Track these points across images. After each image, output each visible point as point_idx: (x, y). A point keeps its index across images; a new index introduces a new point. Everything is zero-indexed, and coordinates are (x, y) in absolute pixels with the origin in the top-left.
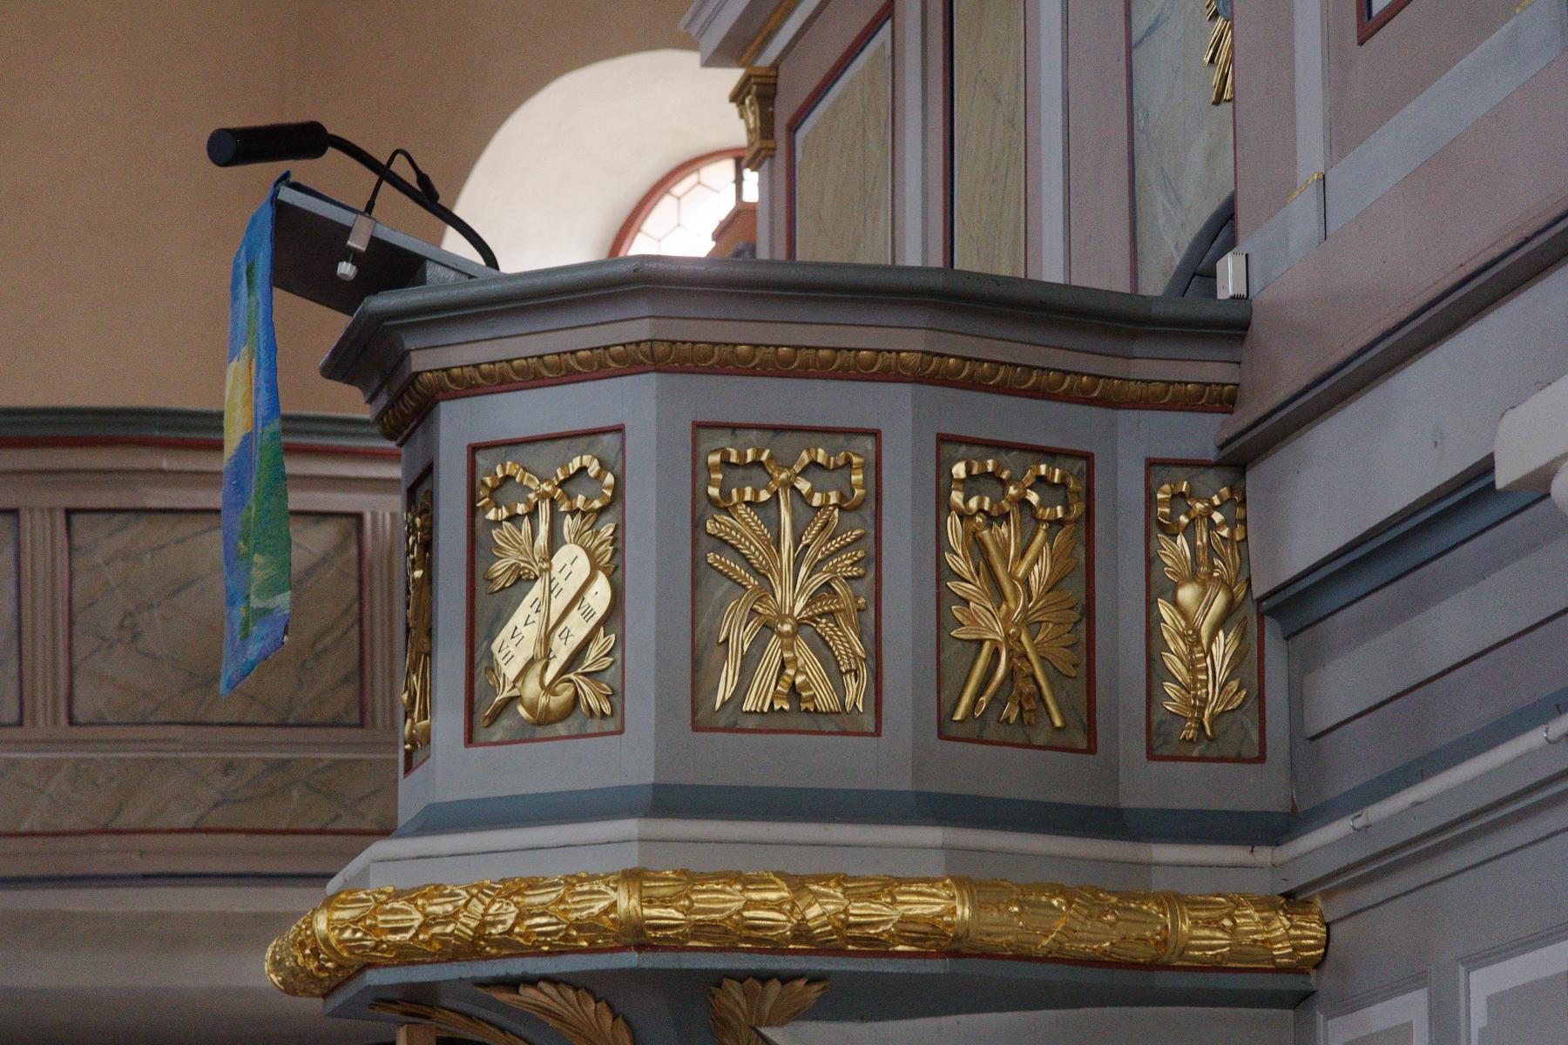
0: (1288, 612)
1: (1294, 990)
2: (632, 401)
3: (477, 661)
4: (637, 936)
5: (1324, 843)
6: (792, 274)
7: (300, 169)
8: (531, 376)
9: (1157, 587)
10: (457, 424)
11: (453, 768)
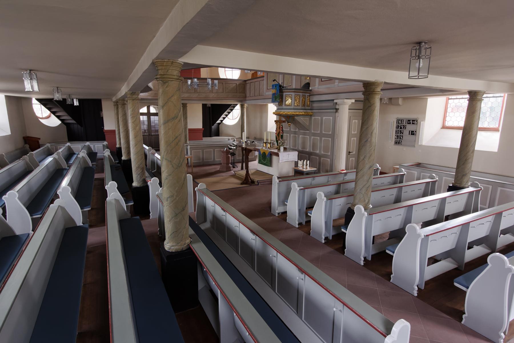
1: (311, 116)
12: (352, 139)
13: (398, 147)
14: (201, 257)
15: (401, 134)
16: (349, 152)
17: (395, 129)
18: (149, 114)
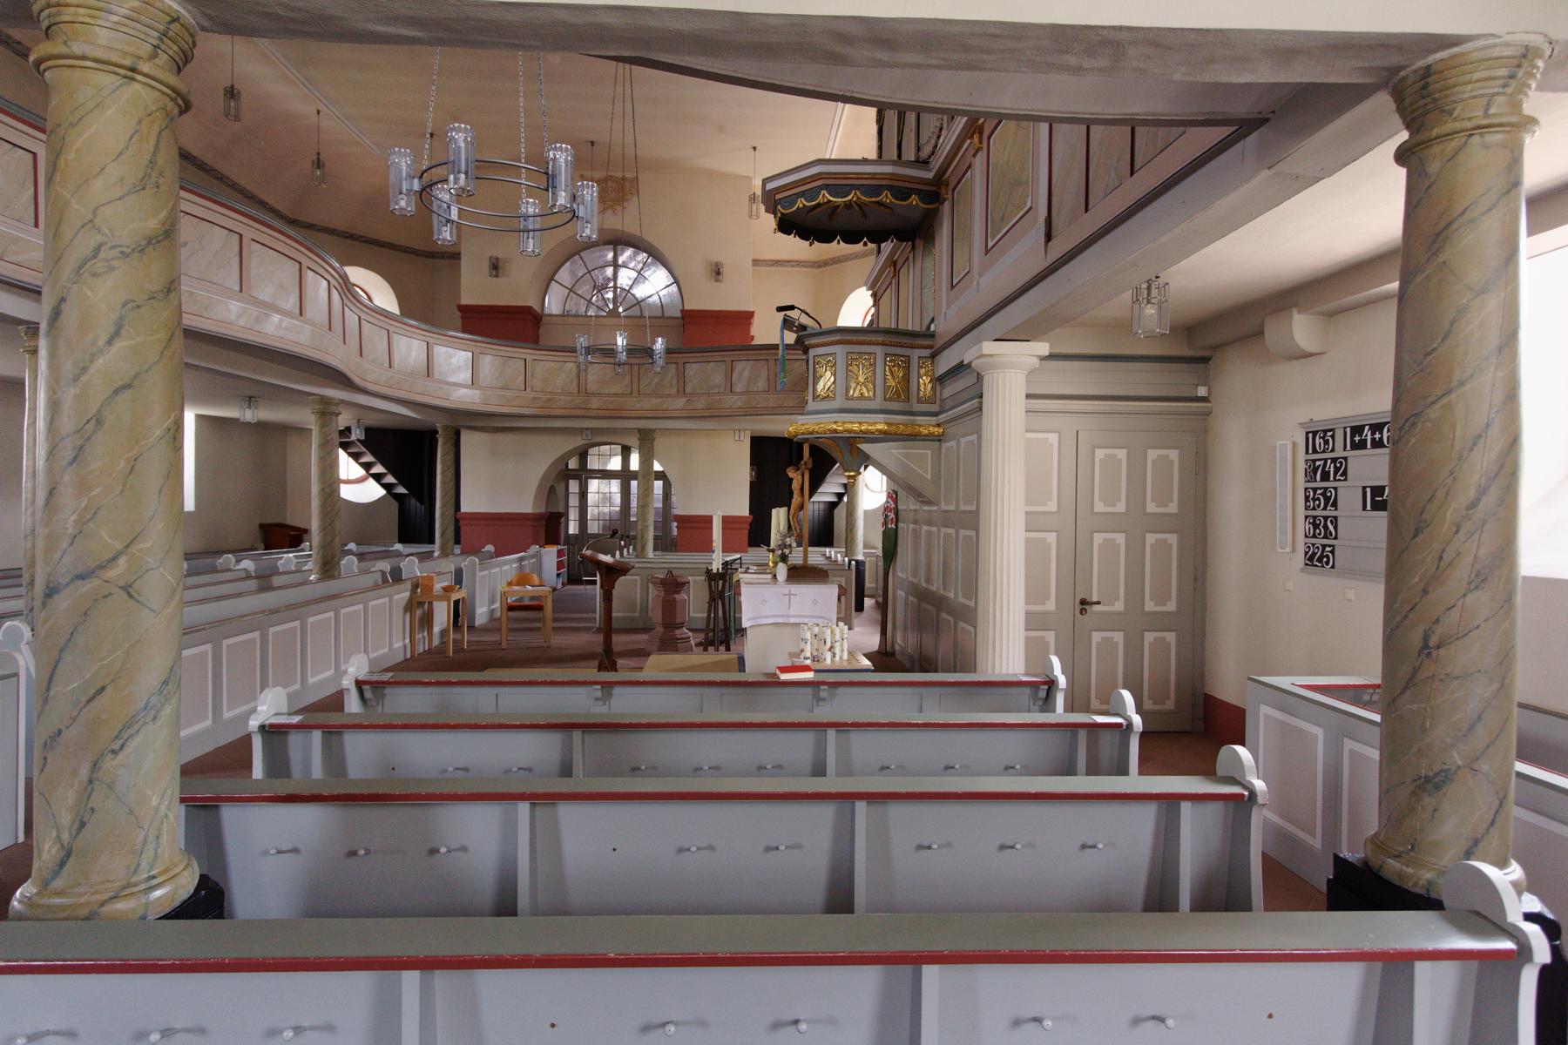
0: (940, 380)
1: (939, 439)
4: (835, 431)
5: (942, 417)
7: (789, 313)
8: (823, 345)
9: (920, 376)
10: (812, 352)
11: (811, 406)
12: (1098, 538)
13: (1321, 580)
14: (159, 955)
15: (1330, 512)
16: (1083, 602)
17: (1301, 483)
18: (625, 476)
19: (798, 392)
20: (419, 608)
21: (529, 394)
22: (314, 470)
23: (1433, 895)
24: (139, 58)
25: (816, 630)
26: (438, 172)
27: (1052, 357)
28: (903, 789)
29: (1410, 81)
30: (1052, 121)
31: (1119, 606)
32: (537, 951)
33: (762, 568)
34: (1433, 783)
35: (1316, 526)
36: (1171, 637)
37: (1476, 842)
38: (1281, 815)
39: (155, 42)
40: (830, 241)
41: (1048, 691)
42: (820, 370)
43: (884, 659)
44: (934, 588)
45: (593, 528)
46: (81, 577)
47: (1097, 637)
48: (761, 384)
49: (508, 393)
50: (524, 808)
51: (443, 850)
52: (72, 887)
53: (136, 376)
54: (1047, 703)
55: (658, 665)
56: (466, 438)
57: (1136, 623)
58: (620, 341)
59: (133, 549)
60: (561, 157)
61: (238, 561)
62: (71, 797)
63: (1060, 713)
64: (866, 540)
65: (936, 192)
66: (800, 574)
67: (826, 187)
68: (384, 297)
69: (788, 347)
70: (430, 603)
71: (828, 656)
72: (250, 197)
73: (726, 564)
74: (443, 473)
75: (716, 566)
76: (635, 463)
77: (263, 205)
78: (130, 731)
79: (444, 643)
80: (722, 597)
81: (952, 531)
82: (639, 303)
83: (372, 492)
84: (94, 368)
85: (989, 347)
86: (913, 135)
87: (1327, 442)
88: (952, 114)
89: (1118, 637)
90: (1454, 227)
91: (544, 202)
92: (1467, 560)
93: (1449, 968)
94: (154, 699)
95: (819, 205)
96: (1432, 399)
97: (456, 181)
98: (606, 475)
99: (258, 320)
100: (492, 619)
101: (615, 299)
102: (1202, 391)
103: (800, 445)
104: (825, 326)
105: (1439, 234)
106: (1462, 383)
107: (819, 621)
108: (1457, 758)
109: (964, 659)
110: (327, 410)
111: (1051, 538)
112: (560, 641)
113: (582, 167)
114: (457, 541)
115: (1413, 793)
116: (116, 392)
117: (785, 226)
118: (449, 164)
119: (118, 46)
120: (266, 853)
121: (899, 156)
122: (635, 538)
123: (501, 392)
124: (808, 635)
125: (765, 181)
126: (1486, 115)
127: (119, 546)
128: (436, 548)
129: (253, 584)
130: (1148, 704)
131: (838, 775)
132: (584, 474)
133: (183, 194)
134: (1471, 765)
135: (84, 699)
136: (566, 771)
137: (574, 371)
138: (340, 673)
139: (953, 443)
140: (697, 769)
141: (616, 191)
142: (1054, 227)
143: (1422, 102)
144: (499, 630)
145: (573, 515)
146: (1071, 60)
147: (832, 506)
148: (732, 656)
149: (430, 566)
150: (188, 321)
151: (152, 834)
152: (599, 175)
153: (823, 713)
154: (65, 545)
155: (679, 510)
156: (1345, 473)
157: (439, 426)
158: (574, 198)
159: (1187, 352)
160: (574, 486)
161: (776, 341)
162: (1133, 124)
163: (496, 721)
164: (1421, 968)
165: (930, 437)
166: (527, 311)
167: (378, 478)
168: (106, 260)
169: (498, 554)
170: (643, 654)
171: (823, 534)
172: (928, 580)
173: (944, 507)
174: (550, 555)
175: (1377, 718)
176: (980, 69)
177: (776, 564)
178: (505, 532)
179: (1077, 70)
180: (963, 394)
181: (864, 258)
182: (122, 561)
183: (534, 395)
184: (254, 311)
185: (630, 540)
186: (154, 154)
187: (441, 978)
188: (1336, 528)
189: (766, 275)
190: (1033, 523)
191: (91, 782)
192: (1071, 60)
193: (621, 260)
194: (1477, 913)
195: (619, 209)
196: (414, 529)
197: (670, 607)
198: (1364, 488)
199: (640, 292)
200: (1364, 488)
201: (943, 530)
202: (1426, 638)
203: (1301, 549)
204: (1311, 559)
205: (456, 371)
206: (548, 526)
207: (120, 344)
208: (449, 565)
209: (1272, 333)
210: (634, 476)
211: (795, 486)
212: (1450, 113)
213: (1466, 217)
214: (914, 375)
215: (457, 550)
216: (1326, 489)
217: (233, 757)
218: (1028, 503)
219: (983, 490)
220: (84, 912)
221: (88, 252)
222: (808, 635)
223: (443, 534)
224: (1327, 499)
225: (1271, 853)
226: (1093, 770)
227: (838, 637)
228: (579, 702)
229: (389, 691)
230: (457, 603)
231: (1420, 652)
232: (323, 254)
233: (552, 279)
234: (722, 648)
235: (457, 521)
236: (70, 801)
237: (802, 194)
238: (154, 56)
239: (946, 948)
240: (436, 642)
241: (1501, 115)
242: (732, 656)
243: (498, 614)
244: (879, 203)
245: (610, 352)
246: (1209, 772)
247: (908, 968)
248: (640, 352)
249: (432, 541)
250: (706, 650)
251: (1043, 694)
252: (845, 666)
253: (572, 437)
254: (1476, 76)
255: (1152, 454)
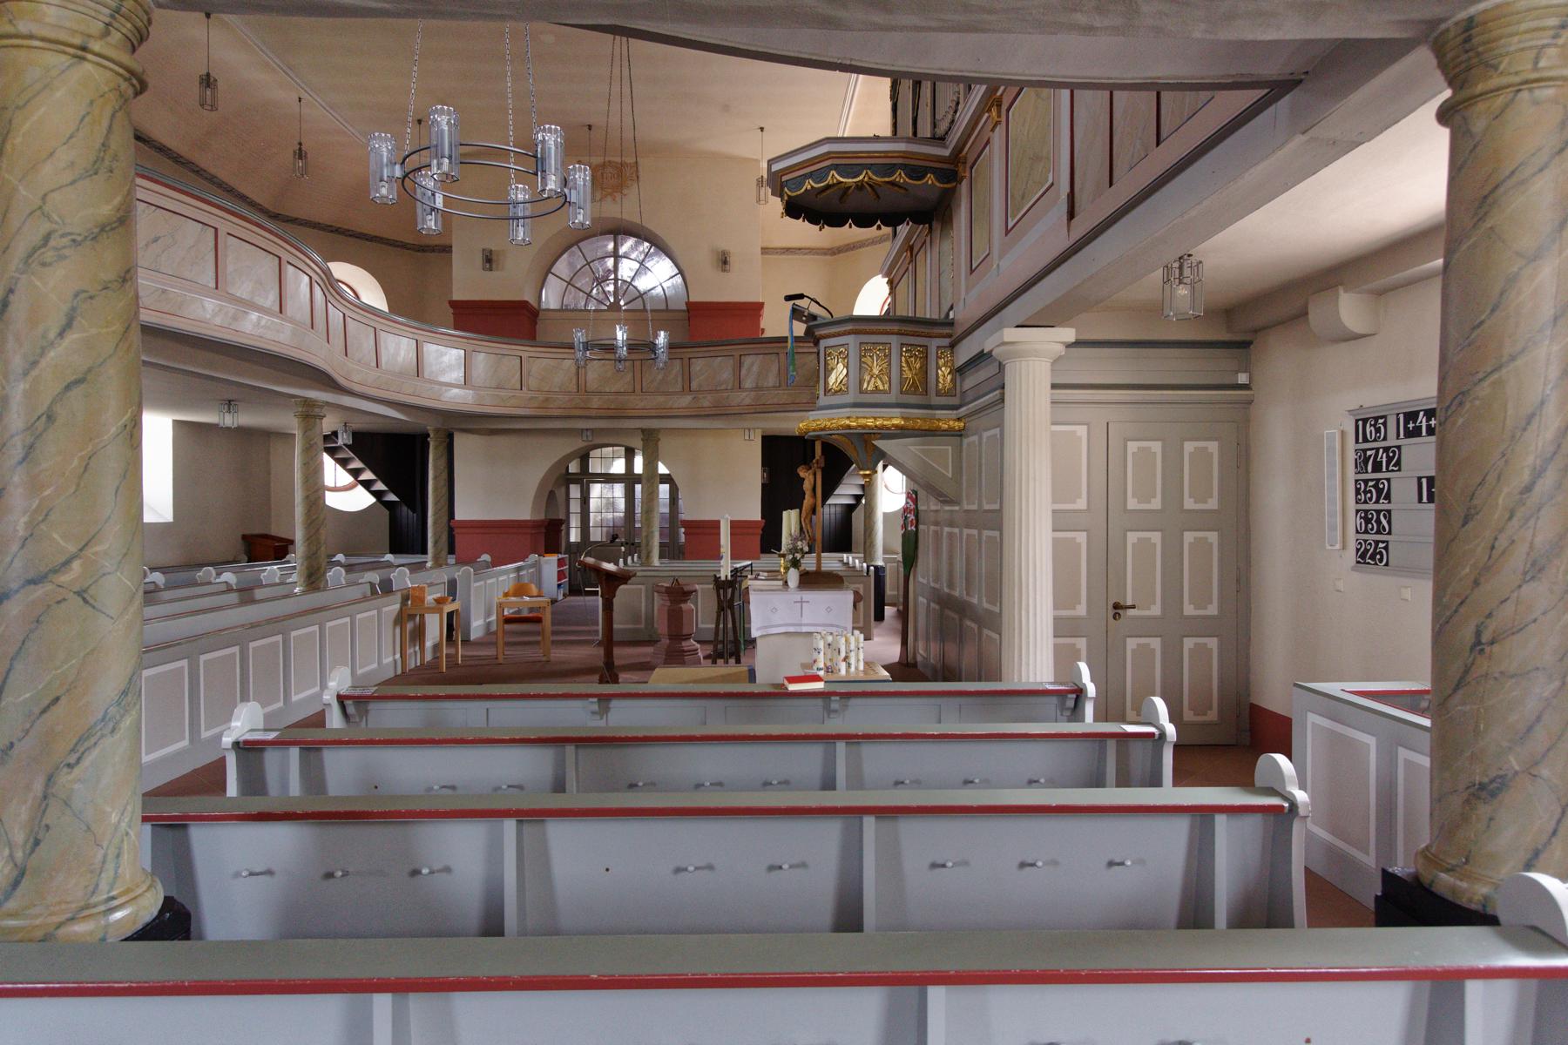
0: (960, 371)
1: (960, 434)
2: (850, 339)
3: (826, 383)
4: (849, 427)
6: (736, 351)
7: (798, 302)
8: (834, 335)
9: (938, 368)
10: (823, 343)
12: (1132, 537)
13: (1375, 579)
16: (1116, 606)
18: (629, 479)
19: (809, 387)
20: (410, 621)
21: (525, 394)
22: (298, 476)
23: (1490, 911)
24: (90, 36)
25: (830, 639)
26: (423, 157)
27: (1078, 344)
28: (914, 803)
29: (1452, 34)
30: (1073, 88)
31: (1156, 610)
32: (515, 972)
33: (773, 574)
34: (1486, 791)
35: (1368, 521)
36: (1213, 643)
37: (1537, 854)
38: (1333, 831)
39: (107, 20)
40: (841, 224)
41: (1077, 700)
42: (832, 363)
43: (904, 669)
44: (957, 593)
45: (596, 535)
46: (33, 582)
47: (1132, 643)
48: (771, 380)
49: (503, 393)
50: (510, 825)
51: (425, 871)
52: (27, 908)
53: (90, 370)
54: (1076, 713)
55: (665, 677)
56: (462, 443)
57: (1173, 627)
58: (621, 335)
59: (89, 552)
60: (551, 139)
61: (219, 574)
62: (24, 815)
63: (1090, 720)
64: (884, 545)
65: (952, 171)
66: (813, 580)
67: (836, 167)
68: (373, 295)
69: (797, 339)
70: (422, 616)
71: (843, 666)
72: (230, 191)
73: (735, 571)
74: (435, 478)
75: (725, 572)
76: (639, 466)
77: (243, 198)
78: (86, 744)
79: (436, 658)
80: (731, 607)
81: (975, 532)
82: (641, 295)
83: (361, 500)
84: (43, 363)
85: (1010, 334)
86: (928, 110)
87: (1378, 430)
88: (969, 83)
89: (1155, 643)
90: (1502, 189)
91: (533, 186)
92: (1521, 551)
93: (1505, 987)
94: (113, 710)
95: (828, 187)
96: (1480, 375)
97: (439, 165)
98: (610, 479)
99: (235, 318)
100: (488, 632)
101: (616, 293)
102: (1242, 378)
103: (812, 442)
104: (838, 315)
105: (1485, 197)
106: (1513, 358)
107: (834, 630)
108: (1514, 763)
109: (989, 668)
110: (310, 413)
111: (1081, 538)
112: (559, 654)
113: (573, 150)
114: (451, 551)
115: (1467, 801)
116: (68, 388)
117: (794, 209)
118: (428, 148)
119: (68, 24)
120: (237, 875)
121: (915, 133)
122: (639, 545)
123: (496, 392)
124: (821, 645)
125: (770, 163)
126: (1535, 68)
127: (72, 548)
128: (429, 559)
129: (233, 597)
130: (1188, 716)
131: (849, 788)
132: (585, 478)
133: (139, 181)
134: (1531, 770)
135: (37, 711)
136: (559, 786)
137: (573, 369)
138: (323, 686)
139: (975, 438)
140: (698, 786)
141: (614, 175)
142: (1077, 205)
143: (1464, 57)
144: (495, 644)
145: (575, 522)
146: (1081, 18)
147: (850, 509)
148: (743, 668)
149: (422, 577)
150: (146, 317)
151: (112, 852)
152: (597, 160)
153: (833, 726)
154: (15, 548)
155: (685, 515)
156: (1398, 463)
157: (430, 429)
158: (565, 182)
159: (1226, 337)
160: (575, 491)
161: (786, 334)
162: (1157, 89)
163: (485, 736)
164: (1473, 988)
165: (951, 433)
166: (523, 306)
167: (367, 485)
168: (57, 249)
169: (495, 564)
170: (648, 667)
171: (841, 537)
172: (951, 585)
173: (966, 507)
174: (550, 565)
175: (1427, 722)
176: (983, 31)
177: (787, 569)
178: (504, 540)
179: (1089, 30)
180: (981, 389)
181: (879, 241)
182: (76, 565)
183: (531, 394)
184: (231, 308)
185: (633, 547)
186: (107, 137)
187: (415, 1001)
188: (1389, 523)
189: (773, 262)
190: (1061, 521)
191: (45, 797)
192: (1081, 18)
193: (622, 250)
194: (1534, 928)
195: (618, 195)
196: (404, 536)
197: (676, 618)
198: (1420, 479)
199: (642, 284)
200: (1420, 479)
201: (966, 531)
202: (1478, 634)
203: (1352, 546)
204: (1363, 556)
205: (448, 369)
206: (549, 534)
207: (73, 337)
208: (443, 575)
209: (1317, 315)
210: (638, 479)
211: (807, 486)
212: (1495, 67)
213: (1514, 179)
214: (932, 365)
215: (451, 560)
216: (1378, 480)
217: (209, 779)
218: (1054, 502)
219: (1006, 484)
220: (39, 934)
221: (37, 239)
222: (821, 645)
223: (436, 543)
224: (1379, 492)
225: (1318, 869)
226: (1124, 781)
227: (853, 647)
228: (574, 715)
229: (372, 706)
230: (450, 615)
231: (1472, 649)
232: (304, 248)
233: (549, 271)
234: (732, 661)
235: (451, 532)
236: (24, 816)
237: (810, 175)
238: (106, 33)
239: (951, 967)
240: (428, 657)
241: (1550, 68)
242: (743, 668)
243: (494, 628)
244: (893, 184)
245: (611, 348)
246: (1245, 780)
247: (913, 990)
248: (641, 347)
249: (424, 552)
250: (714, 662)
251: (1070, 703)
252: (861, 676)
253: (570, 436)
254: (1524, 26)
255: (1189, 447)
